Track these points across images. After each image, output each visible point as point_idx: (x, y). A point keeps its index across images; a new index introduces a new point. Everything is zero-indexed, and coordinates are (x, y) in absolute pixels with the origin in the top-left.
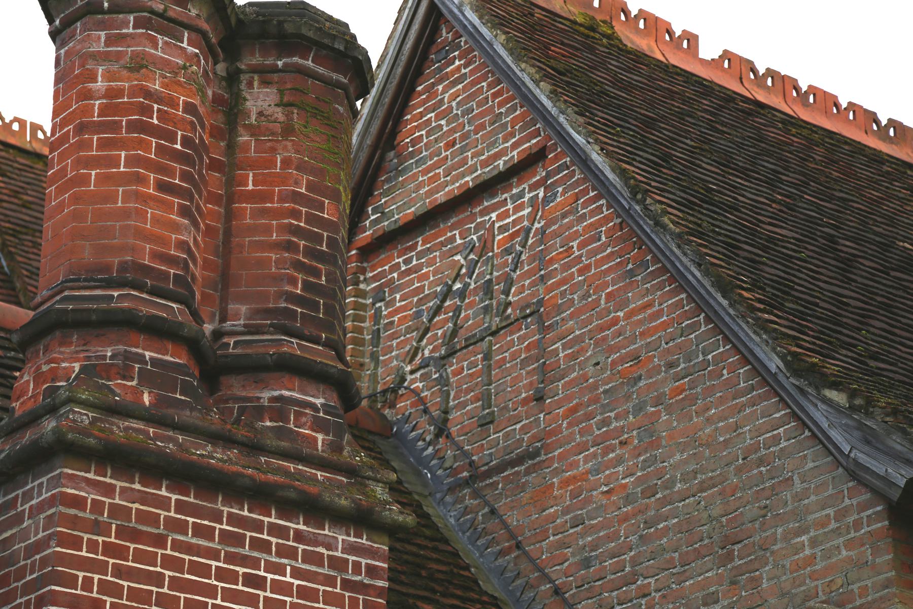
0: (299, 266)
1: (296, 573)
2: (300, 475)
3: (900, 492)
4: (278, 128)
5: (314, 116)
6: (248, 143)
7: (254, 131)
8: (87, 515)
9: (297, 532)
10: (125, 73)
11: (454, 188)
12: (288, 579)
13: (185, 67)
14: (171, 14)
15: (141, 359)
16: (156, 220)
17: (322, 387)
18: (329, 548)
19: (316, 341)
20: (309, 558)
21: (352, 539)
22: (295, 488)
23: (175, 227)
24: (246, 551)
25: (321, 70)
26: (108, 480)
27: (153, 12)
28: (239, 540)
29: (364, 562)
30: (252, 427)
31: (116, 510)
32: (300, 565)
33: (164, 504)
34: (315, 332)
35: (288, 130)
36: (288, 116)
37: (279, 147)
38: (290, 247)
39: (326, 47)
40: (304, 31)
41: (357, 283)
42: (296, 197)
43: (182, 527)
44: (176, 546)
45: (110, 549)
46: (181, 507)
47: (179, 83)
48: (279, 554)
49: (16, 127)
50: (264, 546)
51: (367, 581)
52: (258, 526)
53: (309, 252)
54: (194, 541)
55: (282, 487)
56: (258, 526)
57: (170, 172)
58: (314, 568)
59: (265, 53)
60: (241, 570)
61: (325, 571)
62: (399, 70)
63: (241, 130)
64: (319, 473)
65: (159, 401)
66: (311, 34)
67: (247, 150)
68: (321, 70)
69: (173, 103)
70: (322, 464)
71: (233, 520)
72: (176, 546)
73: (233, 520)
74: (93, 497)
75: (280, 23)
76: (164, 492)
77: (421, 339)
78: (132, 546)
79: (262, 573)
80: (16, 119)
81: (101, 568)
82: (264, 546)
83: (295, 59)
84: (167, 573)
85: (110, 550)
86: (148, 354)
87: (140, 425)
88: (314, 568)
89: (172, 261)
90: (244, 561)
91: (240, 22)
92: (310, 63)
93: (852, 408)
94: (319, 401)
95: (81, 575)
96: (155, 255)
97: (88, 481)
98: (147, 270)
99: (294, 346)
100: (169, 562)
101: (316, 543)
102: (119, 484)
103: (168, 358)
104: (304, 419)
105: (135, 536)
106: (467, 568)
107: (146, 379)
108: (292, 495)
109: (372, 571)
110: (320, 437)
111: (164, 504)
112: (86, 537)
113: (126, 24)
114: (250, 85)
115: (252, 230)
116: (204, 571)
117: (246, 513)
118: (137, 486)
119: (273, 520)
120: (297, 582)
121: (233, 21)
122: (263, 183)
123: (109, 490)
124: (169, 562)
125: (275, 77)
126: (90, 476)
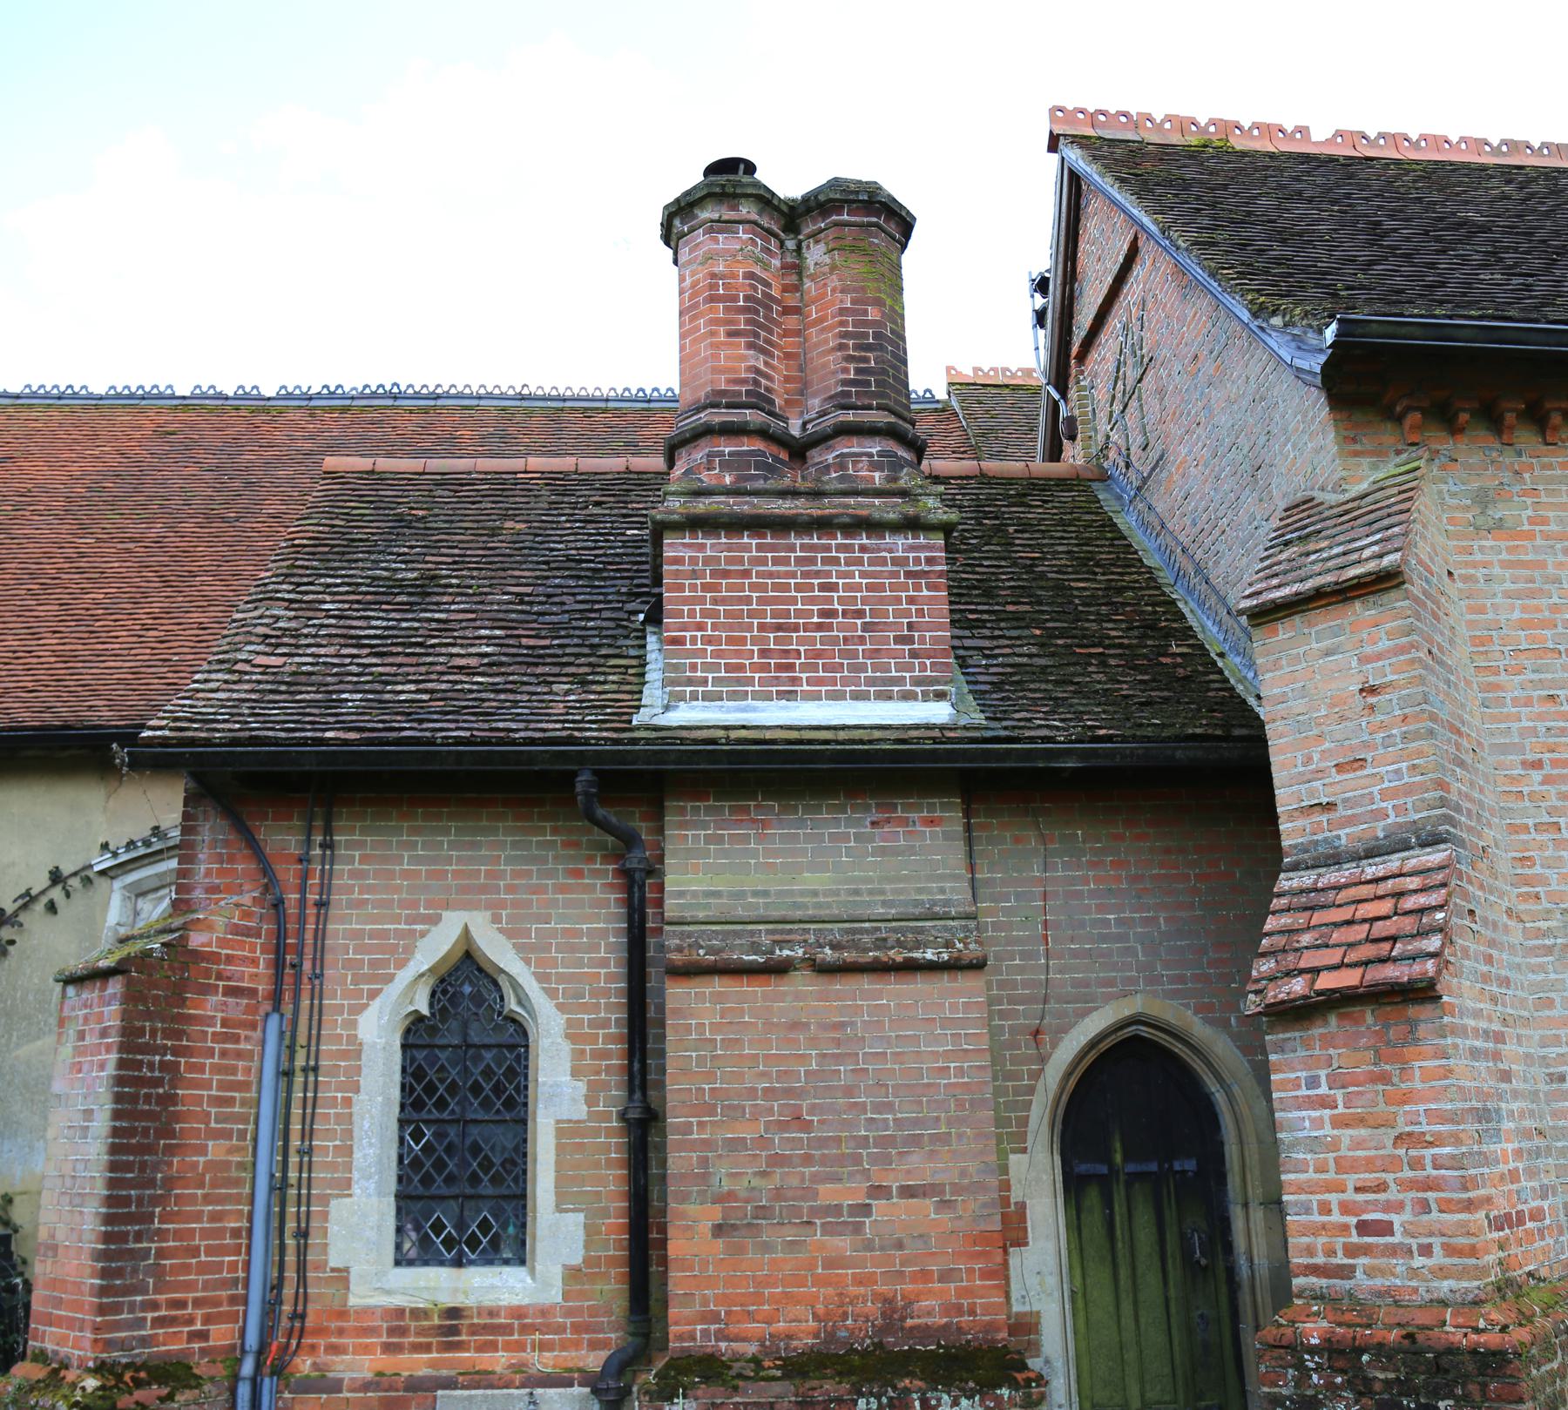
0: (850, 359)
1: (863, 575)
2: (860, 505)
3: (1320, 377)
4: (826, 269)
5: (853, 251)
6: (810, 287)
7: (813, 278)
8: (686, 567)
9: (860, 545)
10: (700, 268)
11: (1105, 290)
12: (857, 580)
13: (742, 249)
14: (725, 217)
15: (722, 454)
16: (727, 358)
17: (877, 439)
18: (890, 551)
19: (869, 408)
20: (872, 562)
21: (910, 541)
22: (847, 515)
23: (743, 358)
24: (819, 567)
25: (853, 219)
26: (700, 541)
27: (712, 221)
28: (813, 561)
29: (922, 555)
30: (818, 480)
31: (707, 560)
32: (866, 568)
33: (747, 548)
34: (866, 402)
35: (833, 268)
36: (832, 259)
37: (828, 281)
38: (842, 347)
39: (854, 201)
40: (832, 196)
41: (1078, 382)
42: (842, 311)
43: (764, 562)
44: (759, 575)
45: (706, 587)
46: (760, 548)
47: (738, 262)
48: (847, 564)
49: (992, 373)
50: (836, 561)
51: (927, 569)
52: (828, 548)
53: (857, 347)
54: (774, 568)
55: (837, 516)
56: (828, 548)
57: (736, 322)
58: (878, 568)
59: (815, 222)
60: (816, 582)
61: (890, 568)
62: (1063, 224)
63: (805, 280)
64: (876, 501)
65: (739, 479)
66: (838, 196)
67: (810, 292)
68: (853, 219)
69: (734, 276)
70: (879, 493)
71: (803, 548)
72: (759, 575)
73: (803, 548)
74: (688, 554)
75: (816, 197)
76: (746, 540)
77: (1111, 405)
78: (724, 582)
79: (834, 580)
80: (992, 369)
81: (702, 601)
82: (836, 561)
83: (834, 217)
84: (754, 595)
85: (706, 587)
86: (727, 450)
87: (722, 498)
88: (878, 568)
89: (744, 381)
90: (817, 574)
91: (792, 208)
92: (846, 217)
93: (1286, 325)
94: (874, 451)
95: (686, 608)
96: (729, 381)
97: (684, 545)
98: (723, 393)
99: (850, 416)
100: (753, 587)
101: (880, 550)
102: (709, 542)
103: (745, 448)
104: (861, 465)
105: (726, 574)
106: (1136, 552)
107: (725, 466)
108: (847, 520)
109: (930, 561)
110: (877, 475)
111: (747, 548)
112: (687, 582)
113: (698, 236)
114: (808, 247)
115: (817, 345)
116: (787, 587)
117: (816, 541)
118: (724, 540)
119: (839, 541)
120: (864, 581)
121: (784, 208)
122: (822, 310)
123: (702, 547)
124: (753, 587)
125: (822, 235)
126: (687, 541)
